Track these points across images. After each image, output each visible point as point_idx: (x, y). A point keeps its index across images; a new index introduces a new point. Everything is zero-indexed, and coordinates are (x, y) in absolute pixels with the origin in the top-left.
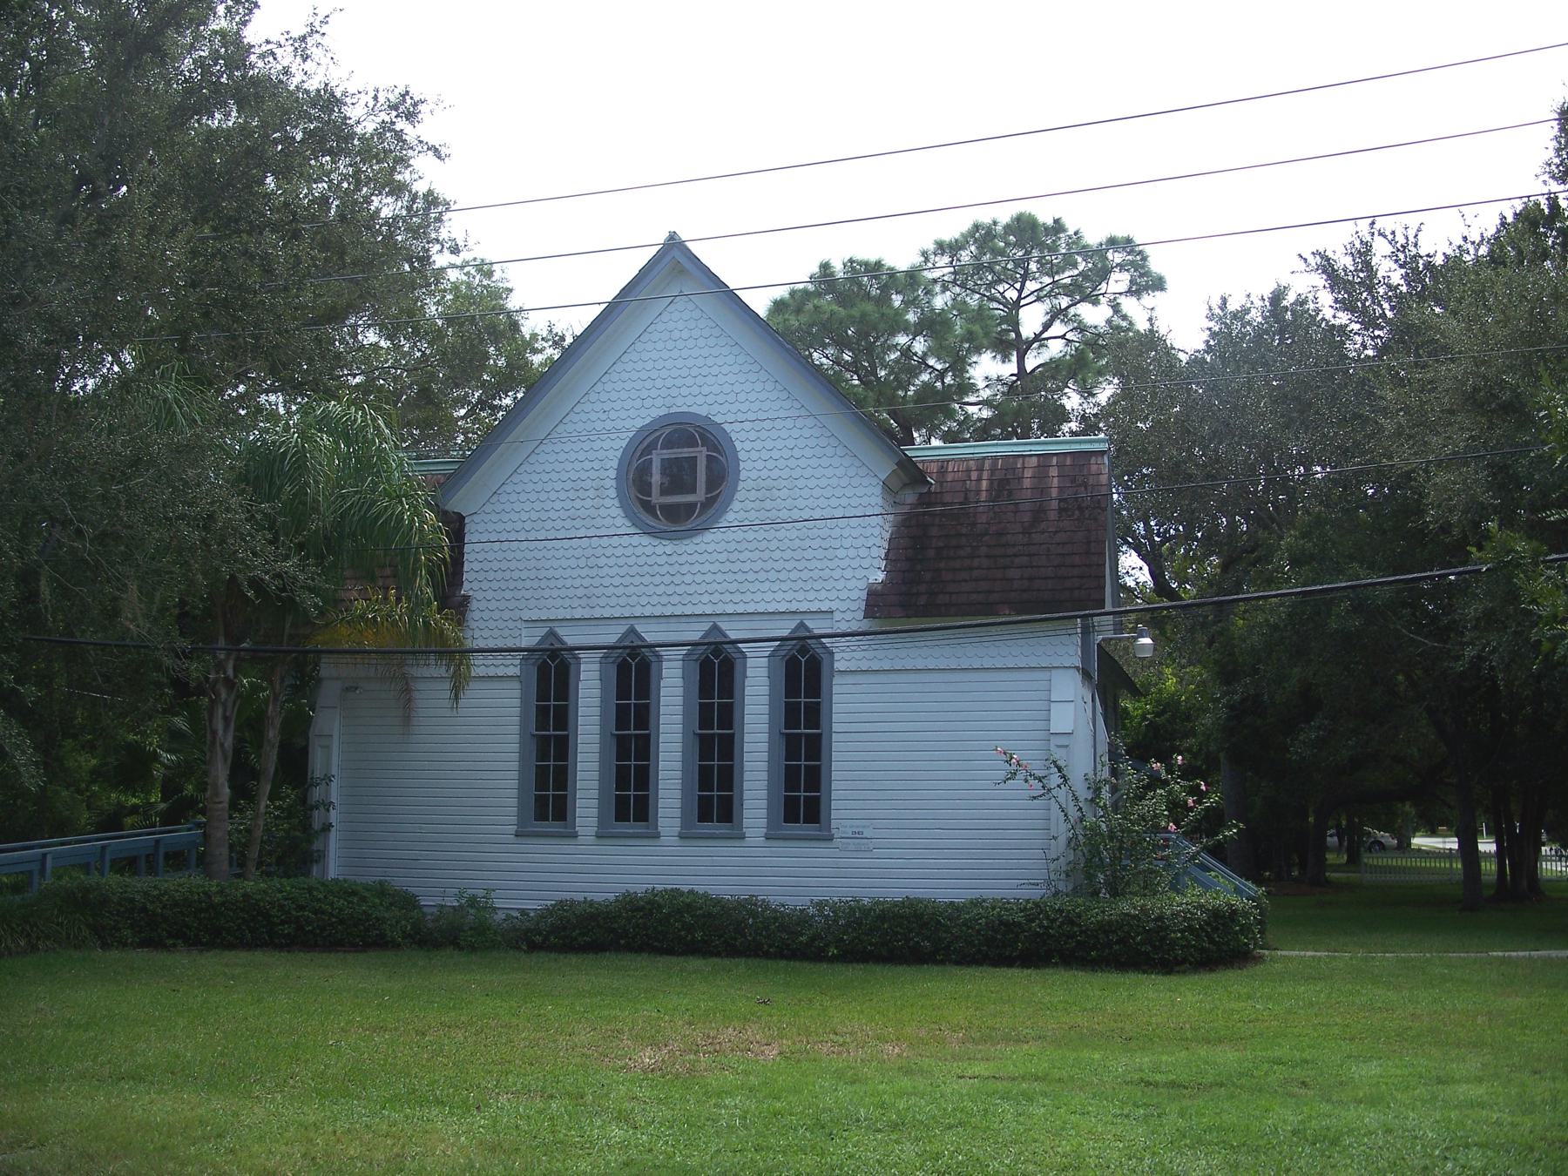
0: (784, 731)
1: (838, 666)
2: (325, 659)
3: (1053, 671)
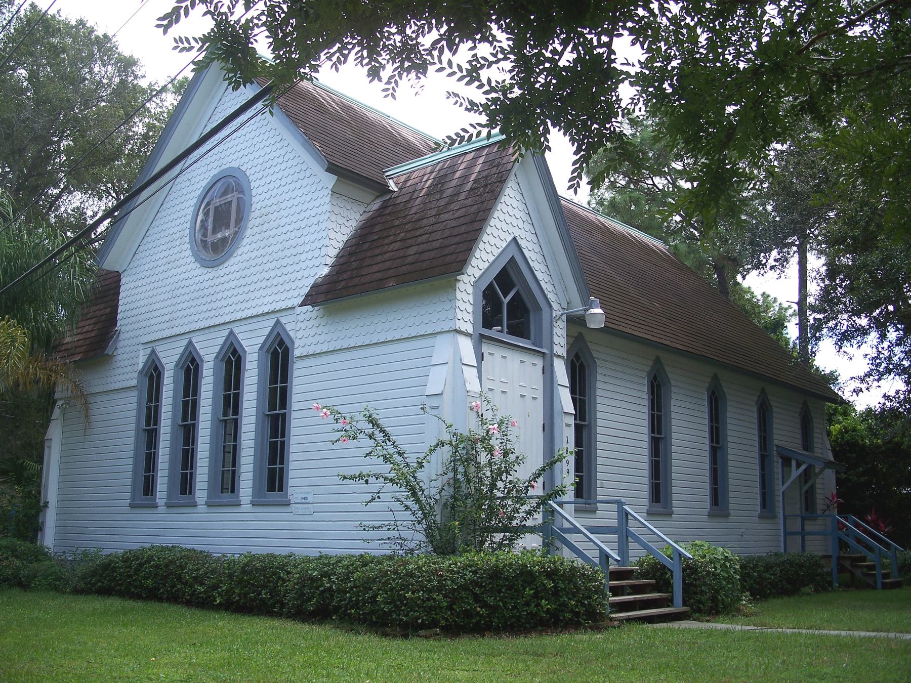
0: (268, 413)
1: (297, 353)
2: (539, 362)
3: (439, 337)
